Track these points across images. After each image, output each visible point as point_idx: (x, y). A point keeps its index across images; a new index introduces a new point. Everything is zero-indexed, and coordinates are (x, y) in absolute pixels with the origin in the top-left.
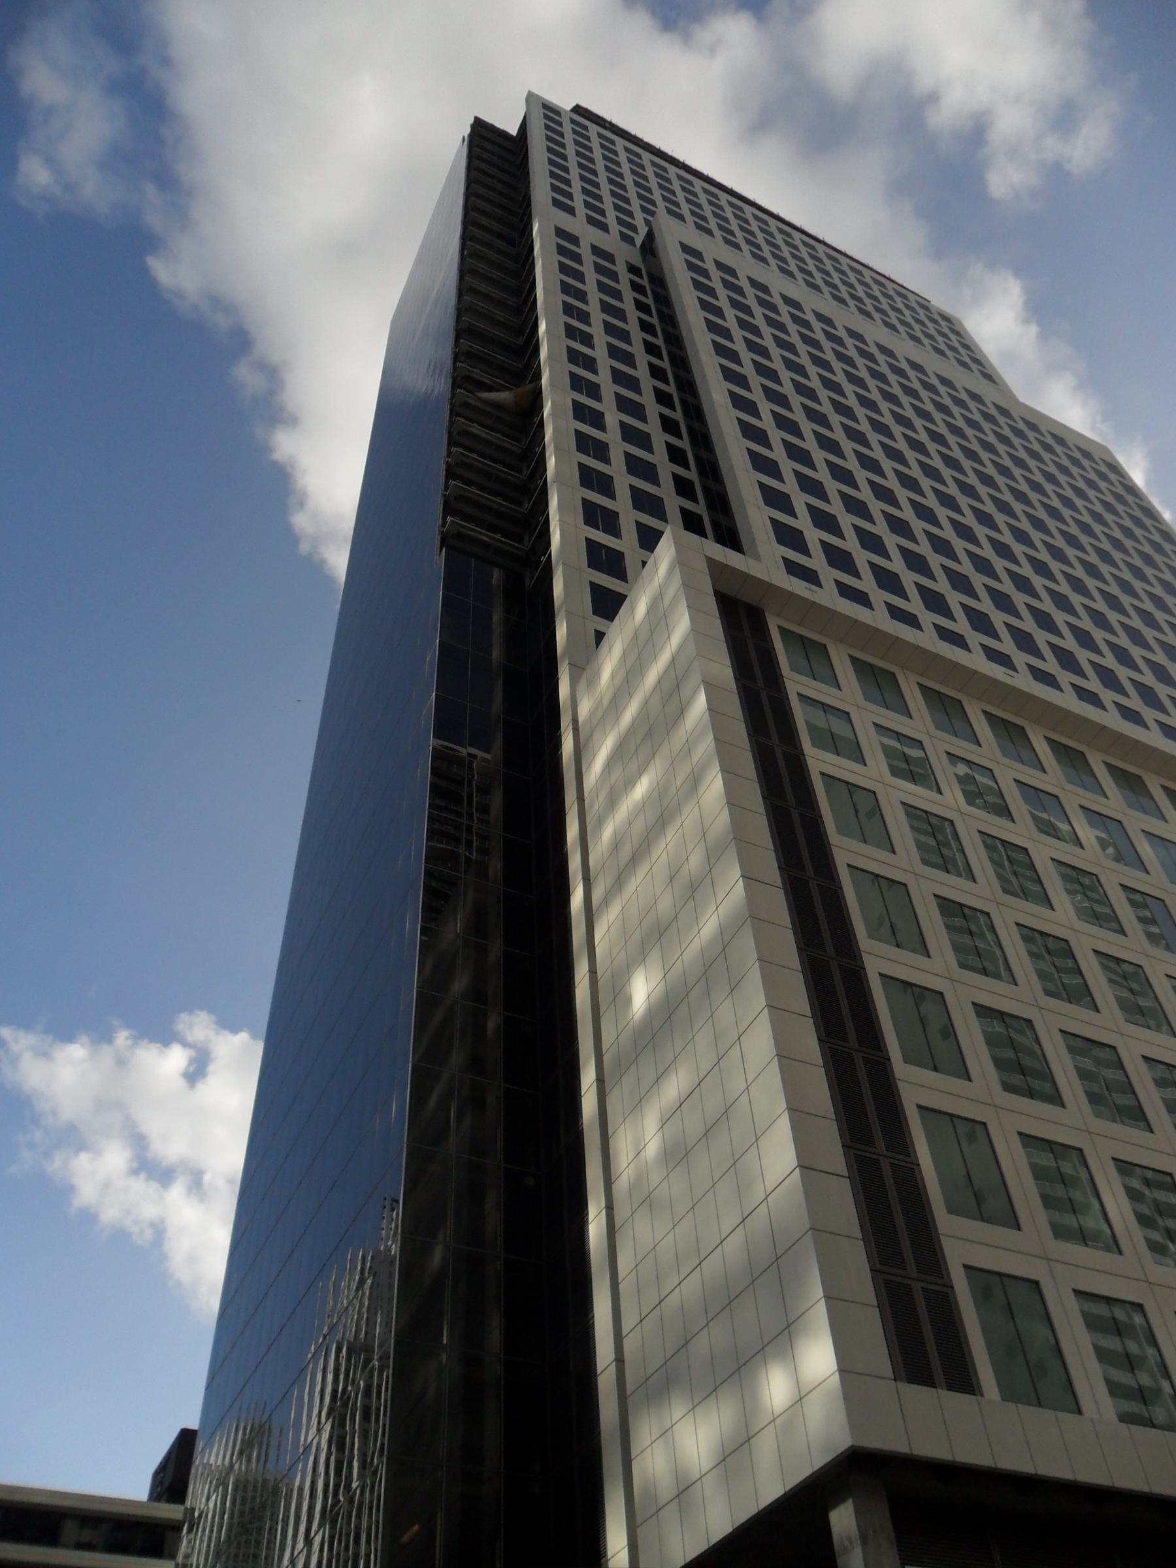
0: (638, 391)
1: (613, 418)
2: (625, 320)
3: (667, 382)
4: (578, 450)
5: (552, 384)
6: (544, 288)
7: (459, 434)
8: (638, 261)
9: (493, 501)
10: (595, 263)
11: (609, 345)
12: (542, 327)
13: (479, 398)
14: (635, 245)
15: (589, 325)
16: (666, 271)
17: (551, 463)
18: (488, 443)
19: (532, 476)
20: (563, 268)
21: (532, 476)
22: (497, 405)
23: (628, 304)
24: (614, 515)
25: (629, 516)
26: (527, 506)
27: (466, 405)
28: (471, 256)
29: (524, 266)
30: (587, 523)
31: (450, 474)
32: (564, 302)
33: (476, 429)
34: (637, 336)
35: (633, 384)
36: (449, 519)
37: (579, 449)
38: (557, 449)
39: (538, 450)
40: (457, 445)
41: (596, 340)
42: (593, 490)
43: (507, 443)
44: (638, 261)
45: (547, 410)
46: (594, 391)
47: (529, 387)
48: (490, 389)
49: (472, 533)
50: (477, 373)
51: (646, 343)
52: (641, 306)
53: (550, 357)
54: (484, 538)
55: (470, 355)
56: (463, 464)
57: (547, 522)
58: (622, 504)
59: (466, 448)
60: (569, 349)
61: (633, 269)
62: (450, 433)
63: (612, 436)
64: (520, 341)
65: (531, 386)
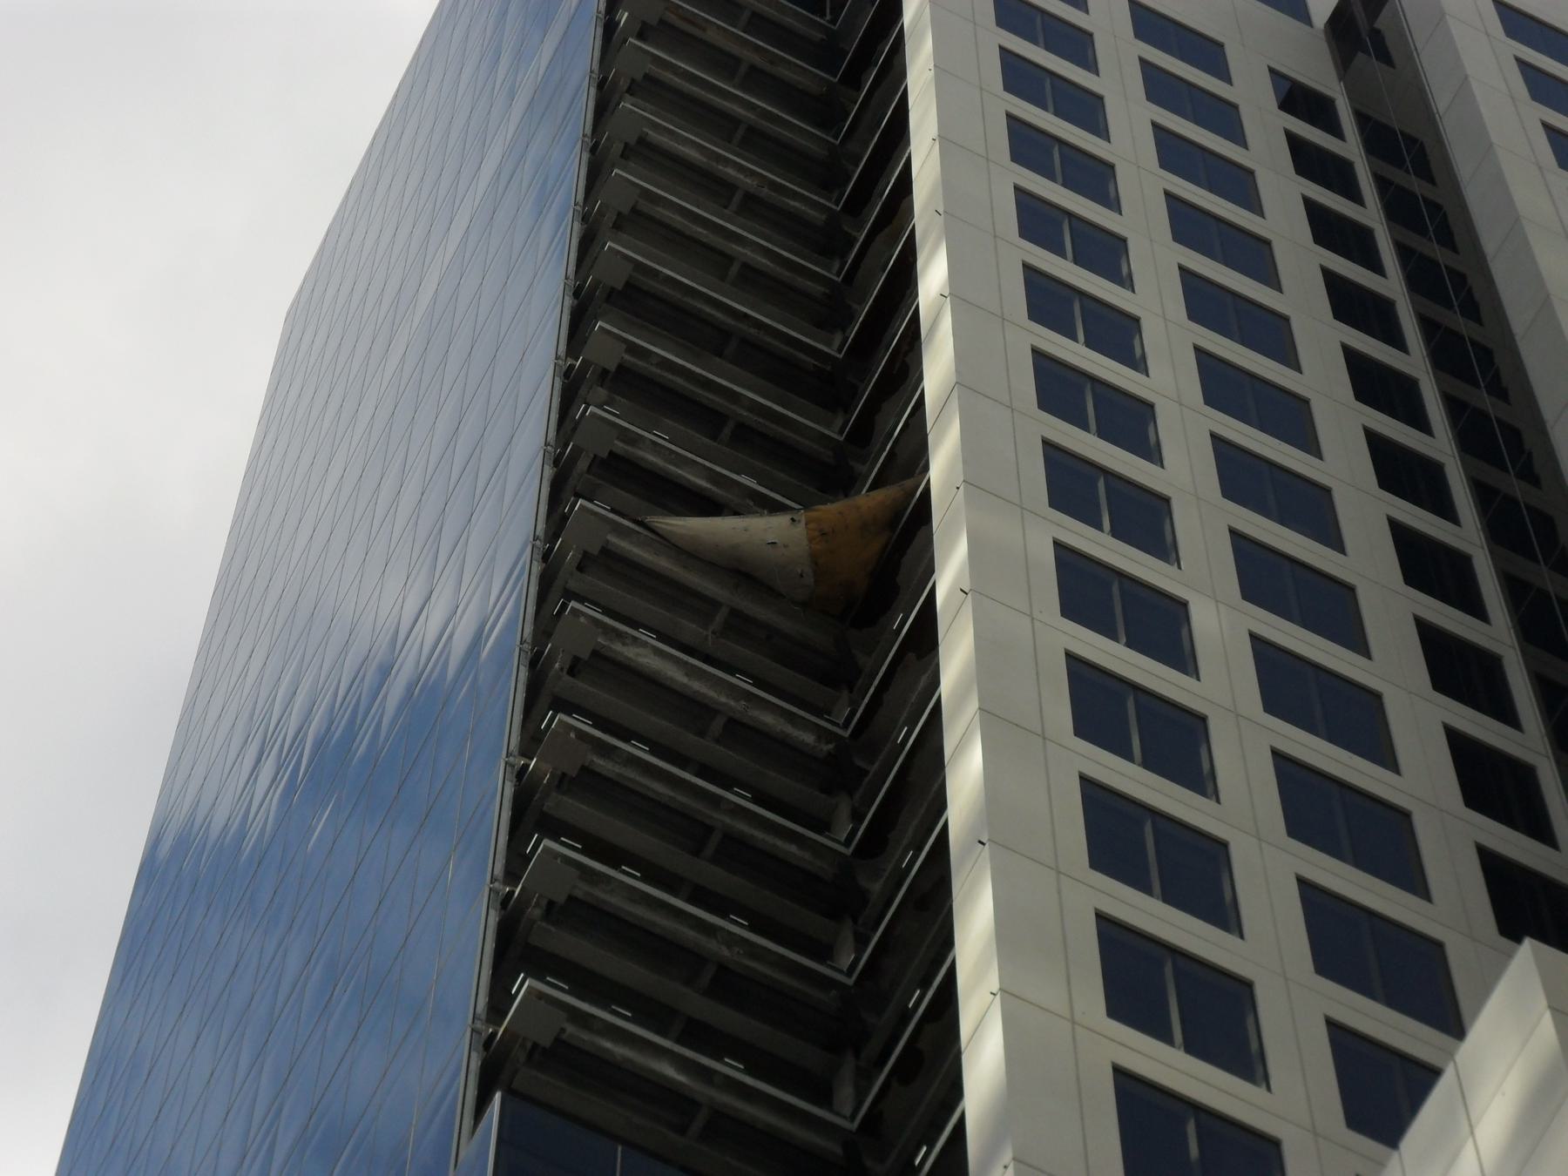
0: (1407, 871)
1: (1222, 621)
2: (1354, 637)
3: (1505, 713)
4: (1080, 732)
5: (973, 481)
6: (945, 140)
7: (574, 669)
8: (1321, 75)
9: (715, 801)
10: (1203, 356)
11: (1223, 448)
12: (933, 277)
13: (665, 542)
14: (1303, 16)
15: (1127, 282)
16: (1441, 101)
17: (966, 773)
18: (694, 711)
19: (875, 844)
20: (1037, 220)
21: (875, 844)
22: (740, 570)
23: (1319, 367)
24: (1215, 852)
25: (1298, 1006)
26: (847, 961)
27: (608, 561)
28: (620, 224)
29: (852, 80)
30: (1116, 1010)
31: (513, 948)
32: (1089, 785)
33: (646, 653)
34: (1366, 510)
35: (1357, 719)
36: (523, 986)
37: (1071, 609)
38: (993, 720)
39: (921, 1001)
40: (542, 963)
41: (1153, 337)
42: (1144, 887)
43: (765, 1102)
44: (1321, 75)
45: (950, 573)
46: (1177, 742)
47: (868, 501)
48: (708, 506)
49: (620, 1051)
50: (661, 445)
51: (1433, 640)
52: (1373, 384)
53: (965, 382)
54: (669, 1071)
55: (627, 381)
56: (586, 782)
57: (946, 1002)
58: (1267, 947)
59: (594, 846)
60: (1095, 795)
61: (1297, 99)
62: (537, 667)
63: (1241, 808)
64: (834, 347)
65: (881, 495)
